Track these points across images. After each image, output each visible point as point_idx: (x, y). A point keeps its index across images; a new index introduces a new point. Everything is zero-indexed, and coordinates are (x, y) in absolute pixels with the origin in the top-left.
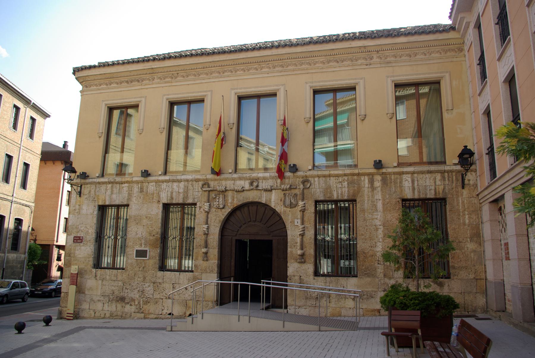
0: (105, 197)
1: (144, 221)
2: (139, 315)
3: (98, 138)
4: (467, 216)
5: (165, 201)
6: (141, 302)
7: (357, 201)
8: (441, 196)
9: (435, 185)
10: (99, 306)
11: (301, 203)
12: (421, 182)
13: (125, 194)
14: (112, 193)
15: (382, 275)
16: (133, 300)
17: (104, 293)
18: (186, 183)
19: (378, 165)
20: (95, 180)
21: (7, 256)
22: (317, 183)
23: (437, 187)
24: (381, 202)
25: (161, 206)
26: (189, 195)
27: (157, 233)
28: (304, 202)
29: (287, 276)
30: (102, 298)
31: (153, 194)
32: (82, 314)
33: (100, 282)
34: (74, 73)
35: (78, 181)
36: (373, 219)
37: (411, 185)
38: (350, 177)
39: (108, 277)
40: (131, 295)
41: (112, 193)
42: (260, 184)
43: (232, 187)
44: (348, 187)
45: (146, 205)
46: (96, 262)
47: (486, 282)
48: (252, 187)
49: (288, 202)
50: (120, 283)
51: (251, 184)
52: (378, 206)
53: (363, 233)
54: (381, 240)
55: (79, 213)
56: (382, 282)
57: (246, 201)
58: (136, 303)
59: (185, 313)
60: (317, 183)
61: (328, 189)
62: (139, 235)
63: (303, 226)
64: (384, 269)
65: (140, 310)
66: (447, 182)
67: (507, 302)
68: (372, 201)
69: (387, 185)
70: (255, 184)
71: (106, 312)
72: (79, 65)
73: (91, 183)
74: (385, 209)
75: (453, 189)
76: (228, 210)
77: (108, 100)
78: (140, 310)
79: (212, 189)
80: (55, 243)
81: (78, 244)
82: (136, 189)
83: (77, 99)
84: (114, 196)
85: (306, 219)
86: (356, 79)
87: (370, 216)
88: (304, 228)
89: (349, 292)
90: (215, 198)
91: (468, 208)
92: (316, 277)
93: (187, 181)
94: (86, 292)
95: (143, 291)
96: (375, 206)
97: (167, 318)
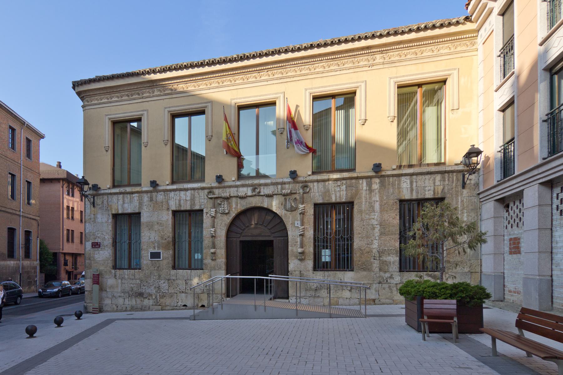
0: (118, 206)
1: (156, 227)
2: (156, 307)
3: (105, 152)
4: (465, 215)
5: (174, 208)
6: (158, 297)
7: (355, 203)
8: (440, 196)
9: (435, 185)
10: (121, 301)
11: (301, 206)
12: (419, 183)
13: (136, 203)
14: (124, 203)
15: (377, 269)
16: (151, 295)
17: (123, 290)
18: (193, 191)
19: (377, 168)
20: (107, 191)
21: (22, 264)
22: (316, 187)
23: (436, 187)
24: (378, 203)
25: (170, 212)
26: (196, 202)
27: (169, 237)
28: (304, 206)
29: (288, 271)
30: (122, 295)
31: (162, 202)
32: (105, 308)
33: (120, 281)
34: (74, 88)
35: (91, 192)
36: (370, 219)
37: (409, 186)
38: (348, 181)
39: (126, 276)
40: (149, 291)
41: (124, 203)
42: (262, 190)
43: (235, 194)
44: (346, 190)
45: (156, 213)
46: (114, 264)
47: (481, 275)
48: (254, 193)
49: (288, 206)
50: (138, 281)
51: (254, 190)
52: (376, 207)
53: (360, 232)
54: (377, 238)
55: (94, 221)
56: (378, 275)
57: (249, 206)
58: (154, 297)
59: (197, 305)
60: (316, 187)
61: (327, 192)
62: (152, 239)
63: (303, 227)
64: (380, 264)
65: (157, 304)
66: (447, 182)
67: (506, 292)
68: (369, 203)
69: (385, 187)
70: (257, 191)
71: (128, 306)
72: (78, 79)
73: (103, 194)
74: (382, 210)
75: (452, 189)
76: (233, 215)
77: (110, 115)
78: (157, 304)
79: (217, 196)
80: (61, 251)
81: (96, 249)
82: (146, 198)
83: (80, 113)
84: (126, 205)
85: (305, 220)
86: (357, 82)
87: (367, 216)
88: (304, 228)
89: (346, 283)
90: (220, 204)
91: (467, 207)
92: (315, 272)
93: (194, 189)
94: (108, 290)
95: (159, 288)
96: (372, 207)
97: (182, 309)
